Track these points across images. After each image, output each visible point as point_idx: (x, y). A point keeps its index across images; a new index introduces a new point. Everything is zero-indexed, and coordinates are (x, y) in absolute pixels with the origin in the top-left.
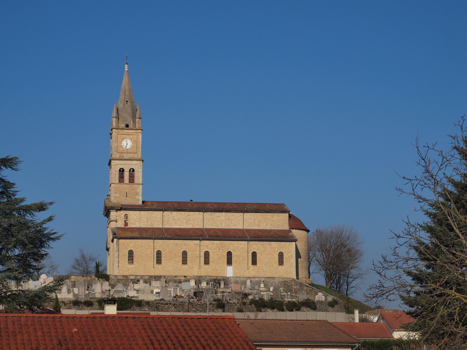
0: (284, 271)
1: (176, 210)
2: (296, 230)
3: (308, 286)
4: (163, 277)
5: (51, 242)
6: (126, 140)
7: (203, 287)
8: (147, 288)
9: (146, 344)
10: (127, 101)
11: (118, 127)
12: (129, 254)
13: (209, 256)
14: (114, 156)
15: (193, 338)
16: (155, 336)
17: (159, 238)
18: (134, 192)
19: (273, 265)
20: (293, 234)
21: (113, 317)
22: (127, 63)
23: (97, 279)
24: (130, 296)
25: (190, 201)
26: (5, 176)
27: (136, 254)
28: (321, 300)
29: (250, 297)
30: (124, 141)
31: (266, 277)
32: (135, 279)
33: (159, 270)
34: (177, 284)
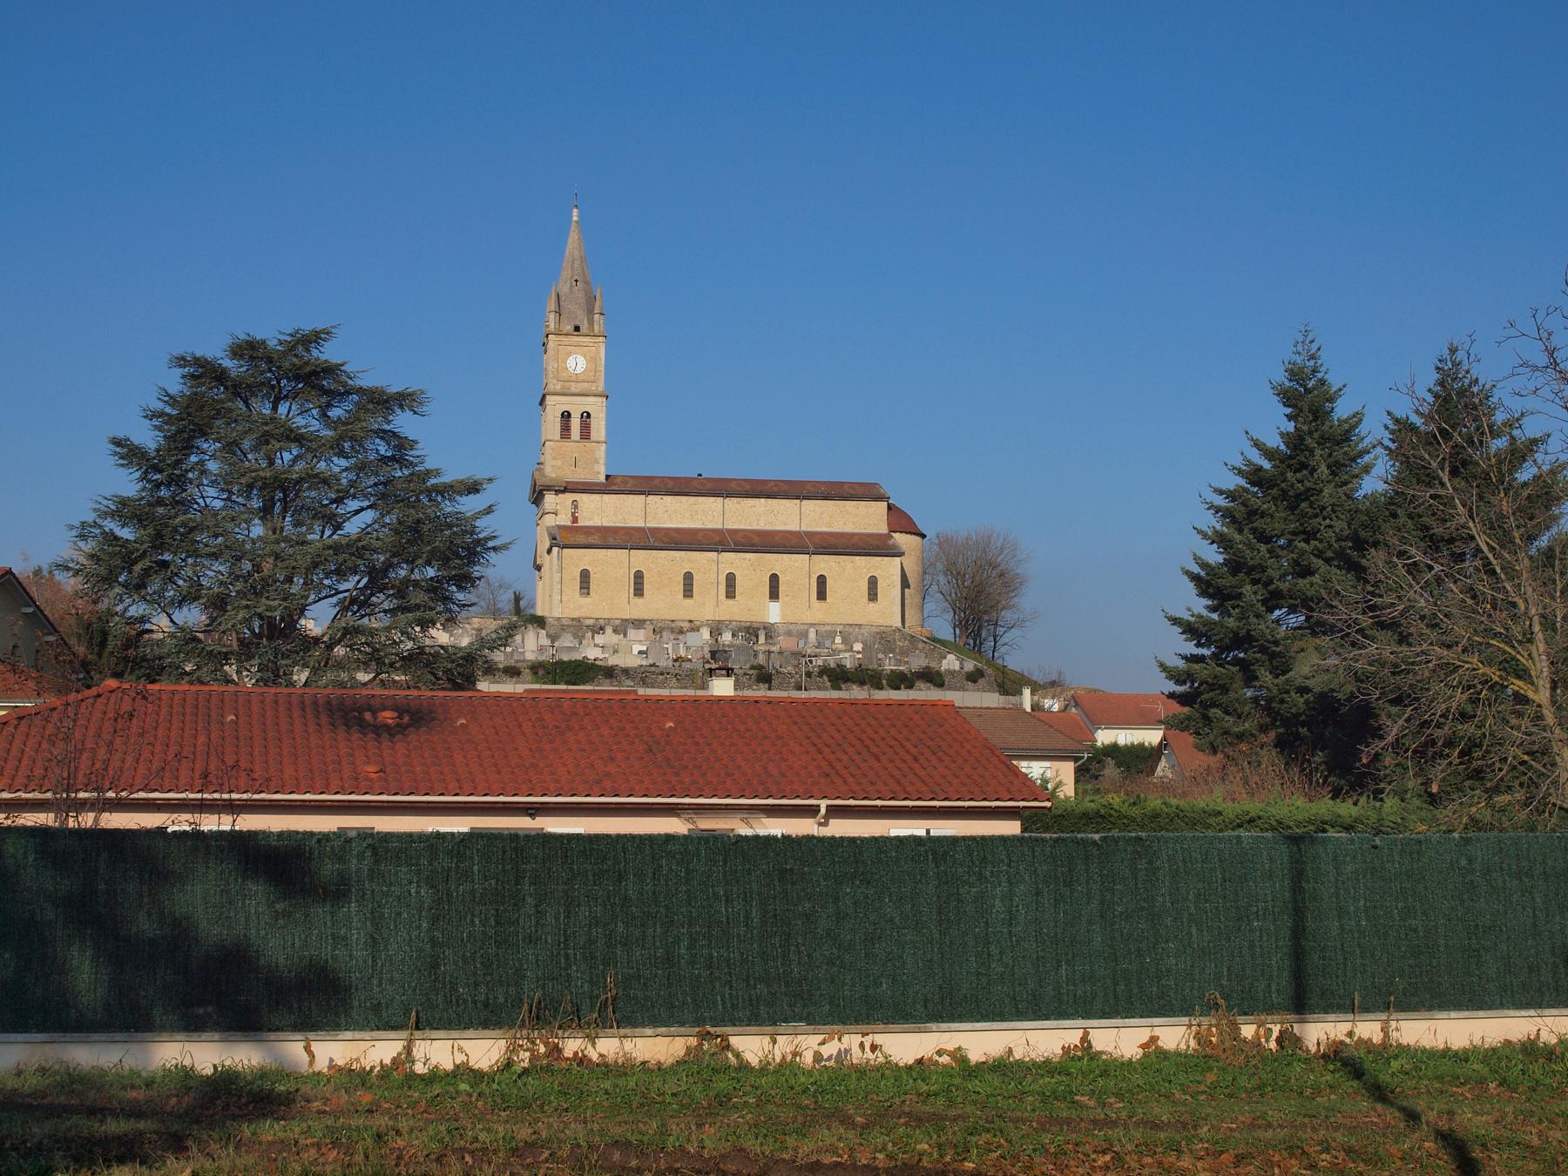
5: (492, 554)
10: (576, 281)
14: (551, 387)
21: (730, 701)
32: (594, 626)
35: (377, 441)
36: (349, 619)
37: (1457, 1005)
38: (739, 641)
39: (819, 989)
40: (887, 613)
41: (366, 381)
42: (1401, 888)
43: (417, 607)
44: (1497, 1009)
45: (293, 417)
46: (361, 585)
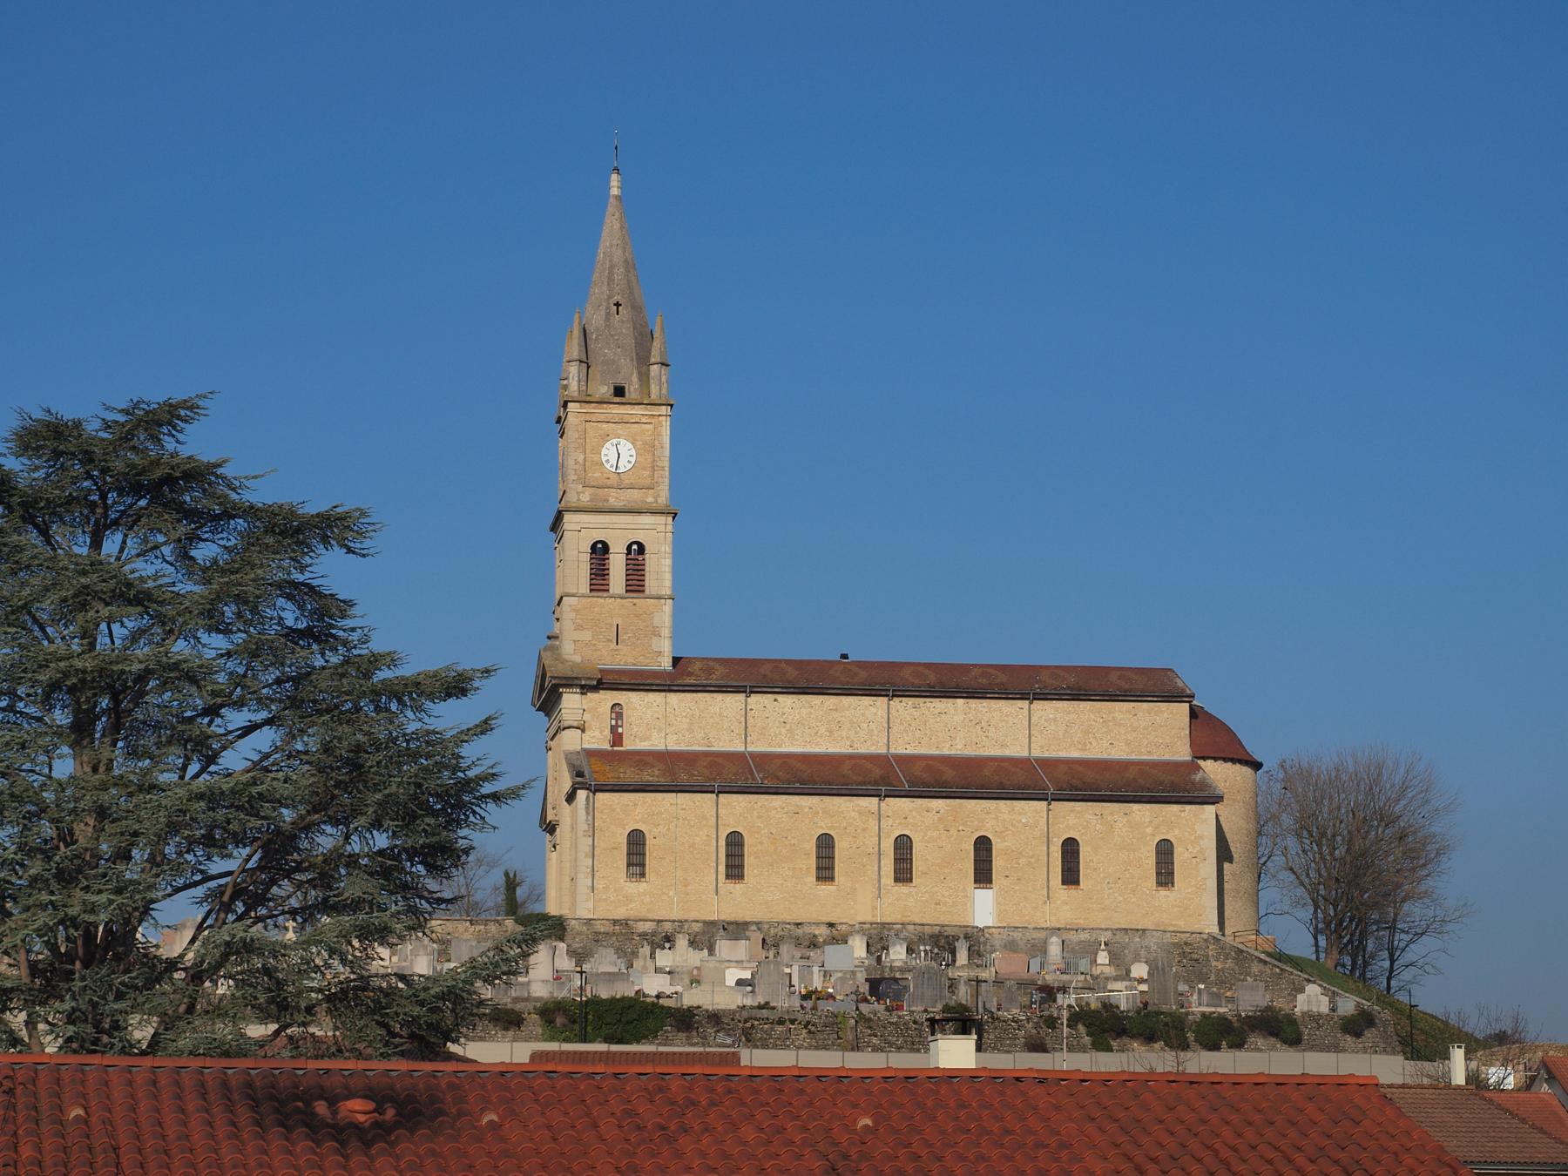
0: (1176, 906)
1: (792, 690)
2: (1215, 761)
3: (1265, 962)
4: (754, 928)
5: (491, 806)
6: (615, 441)
7: (893, 961)
10: (618, 305)
11: (587, 395)
12: (629, 844)
13: (911, 854)
17: (735, 789)
18: (644, 624)
19: (1137, 886)
20: (1205, 775)
22: (616, 170)
25: (838, 658)
26: (322, 577)
27: (654, 845)
28: (1315, 1010)
29: (1066, 1001)
30: (608, 445)
31: (1117, 930)
32: (654, 934)
33: (735, 902)
34: (804, 951)
35: (281, 602)
36: (234, 930)
38: (921, 962)
41: (260, 494)
43: (355, 906)
45: (128, 561)
46: (251, 864)
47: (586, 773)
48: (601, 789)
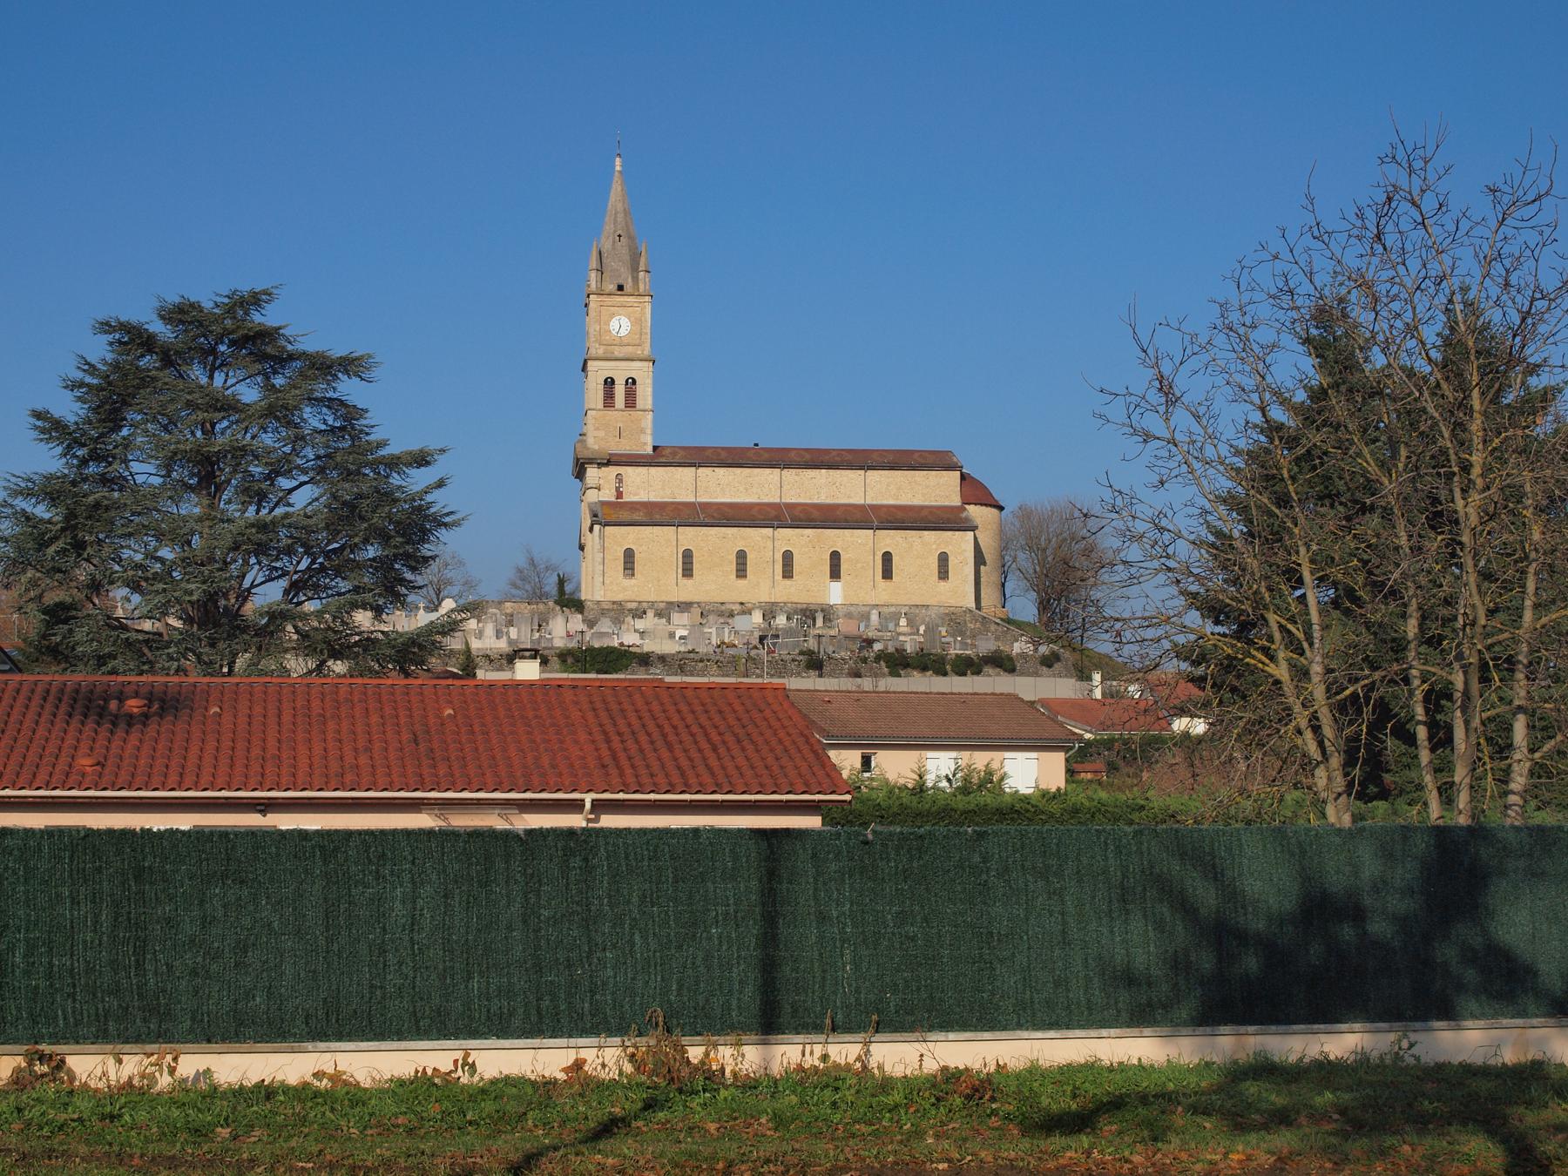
3: (998, 624)
5: (443, 531)
6: (618, 318)
8: (660, 627)
9: (593, 741)
10: (620, 236)
14: (593, 352)
15: (695, 729)
16: (615, 725)
21: (530, 685)
23: (558, 608)
24: (626, 643)
29: (877, 647)
32: (637, 610)
37: (964, 1026)
39: (180, 1002)
40: (958, 592)
41: (309, 345)
42: (897, 890)
44: (1014, 1029)
47: (600, 515)
48: (607, 524)
